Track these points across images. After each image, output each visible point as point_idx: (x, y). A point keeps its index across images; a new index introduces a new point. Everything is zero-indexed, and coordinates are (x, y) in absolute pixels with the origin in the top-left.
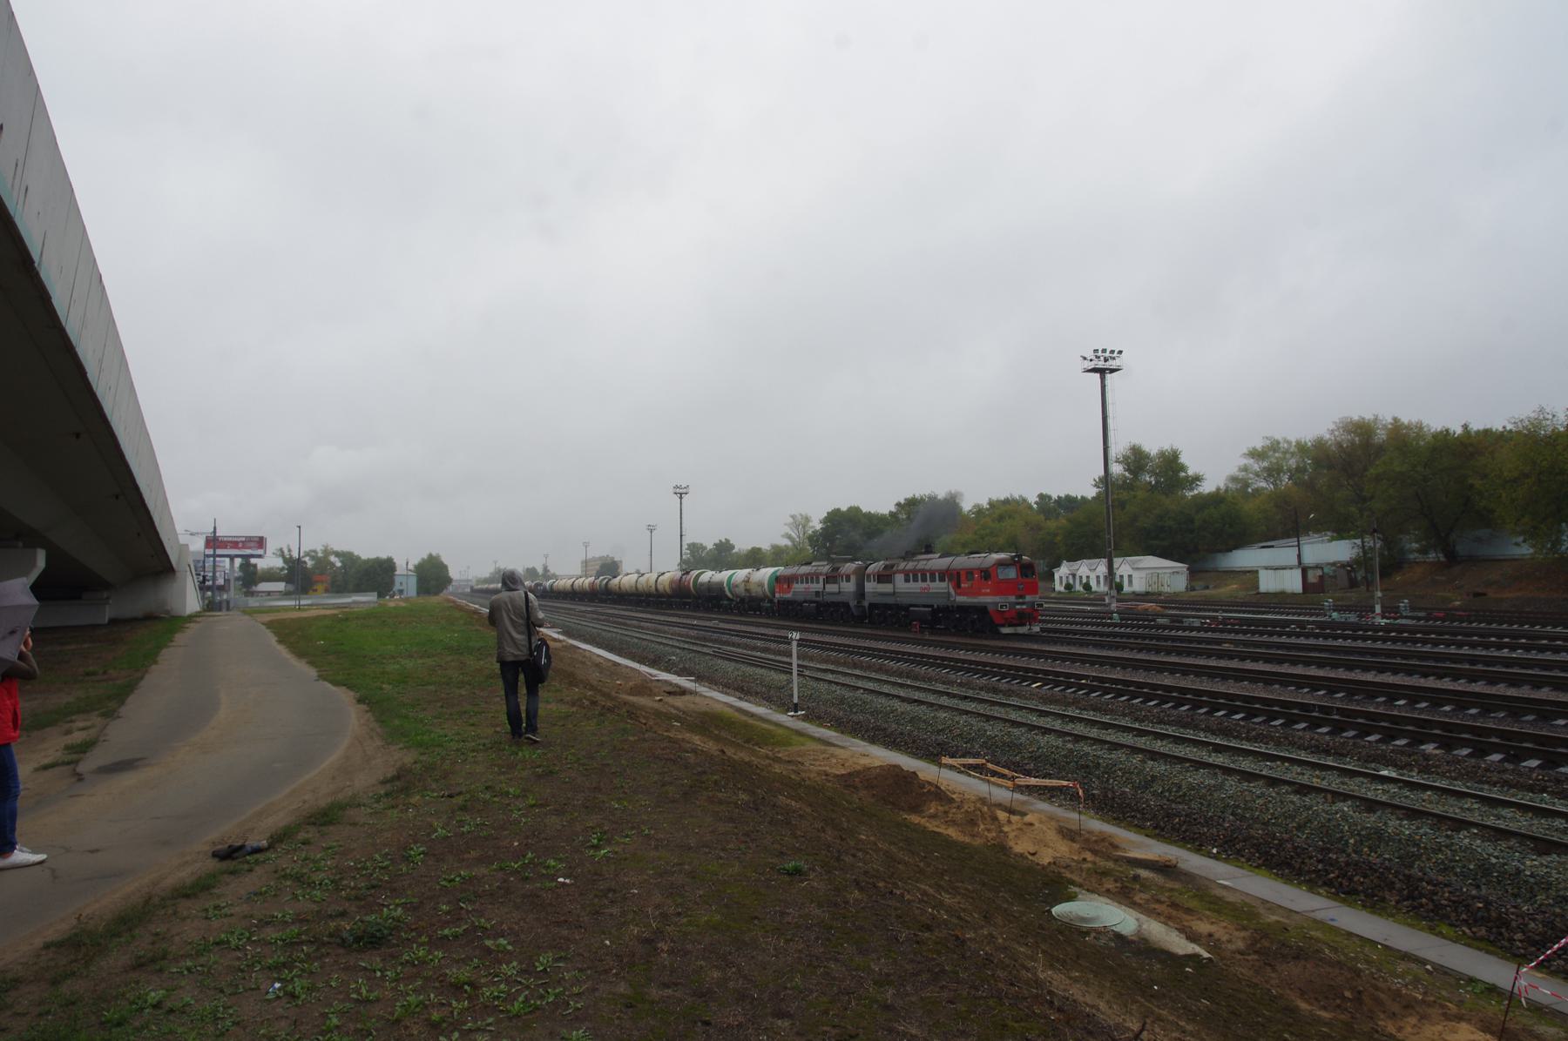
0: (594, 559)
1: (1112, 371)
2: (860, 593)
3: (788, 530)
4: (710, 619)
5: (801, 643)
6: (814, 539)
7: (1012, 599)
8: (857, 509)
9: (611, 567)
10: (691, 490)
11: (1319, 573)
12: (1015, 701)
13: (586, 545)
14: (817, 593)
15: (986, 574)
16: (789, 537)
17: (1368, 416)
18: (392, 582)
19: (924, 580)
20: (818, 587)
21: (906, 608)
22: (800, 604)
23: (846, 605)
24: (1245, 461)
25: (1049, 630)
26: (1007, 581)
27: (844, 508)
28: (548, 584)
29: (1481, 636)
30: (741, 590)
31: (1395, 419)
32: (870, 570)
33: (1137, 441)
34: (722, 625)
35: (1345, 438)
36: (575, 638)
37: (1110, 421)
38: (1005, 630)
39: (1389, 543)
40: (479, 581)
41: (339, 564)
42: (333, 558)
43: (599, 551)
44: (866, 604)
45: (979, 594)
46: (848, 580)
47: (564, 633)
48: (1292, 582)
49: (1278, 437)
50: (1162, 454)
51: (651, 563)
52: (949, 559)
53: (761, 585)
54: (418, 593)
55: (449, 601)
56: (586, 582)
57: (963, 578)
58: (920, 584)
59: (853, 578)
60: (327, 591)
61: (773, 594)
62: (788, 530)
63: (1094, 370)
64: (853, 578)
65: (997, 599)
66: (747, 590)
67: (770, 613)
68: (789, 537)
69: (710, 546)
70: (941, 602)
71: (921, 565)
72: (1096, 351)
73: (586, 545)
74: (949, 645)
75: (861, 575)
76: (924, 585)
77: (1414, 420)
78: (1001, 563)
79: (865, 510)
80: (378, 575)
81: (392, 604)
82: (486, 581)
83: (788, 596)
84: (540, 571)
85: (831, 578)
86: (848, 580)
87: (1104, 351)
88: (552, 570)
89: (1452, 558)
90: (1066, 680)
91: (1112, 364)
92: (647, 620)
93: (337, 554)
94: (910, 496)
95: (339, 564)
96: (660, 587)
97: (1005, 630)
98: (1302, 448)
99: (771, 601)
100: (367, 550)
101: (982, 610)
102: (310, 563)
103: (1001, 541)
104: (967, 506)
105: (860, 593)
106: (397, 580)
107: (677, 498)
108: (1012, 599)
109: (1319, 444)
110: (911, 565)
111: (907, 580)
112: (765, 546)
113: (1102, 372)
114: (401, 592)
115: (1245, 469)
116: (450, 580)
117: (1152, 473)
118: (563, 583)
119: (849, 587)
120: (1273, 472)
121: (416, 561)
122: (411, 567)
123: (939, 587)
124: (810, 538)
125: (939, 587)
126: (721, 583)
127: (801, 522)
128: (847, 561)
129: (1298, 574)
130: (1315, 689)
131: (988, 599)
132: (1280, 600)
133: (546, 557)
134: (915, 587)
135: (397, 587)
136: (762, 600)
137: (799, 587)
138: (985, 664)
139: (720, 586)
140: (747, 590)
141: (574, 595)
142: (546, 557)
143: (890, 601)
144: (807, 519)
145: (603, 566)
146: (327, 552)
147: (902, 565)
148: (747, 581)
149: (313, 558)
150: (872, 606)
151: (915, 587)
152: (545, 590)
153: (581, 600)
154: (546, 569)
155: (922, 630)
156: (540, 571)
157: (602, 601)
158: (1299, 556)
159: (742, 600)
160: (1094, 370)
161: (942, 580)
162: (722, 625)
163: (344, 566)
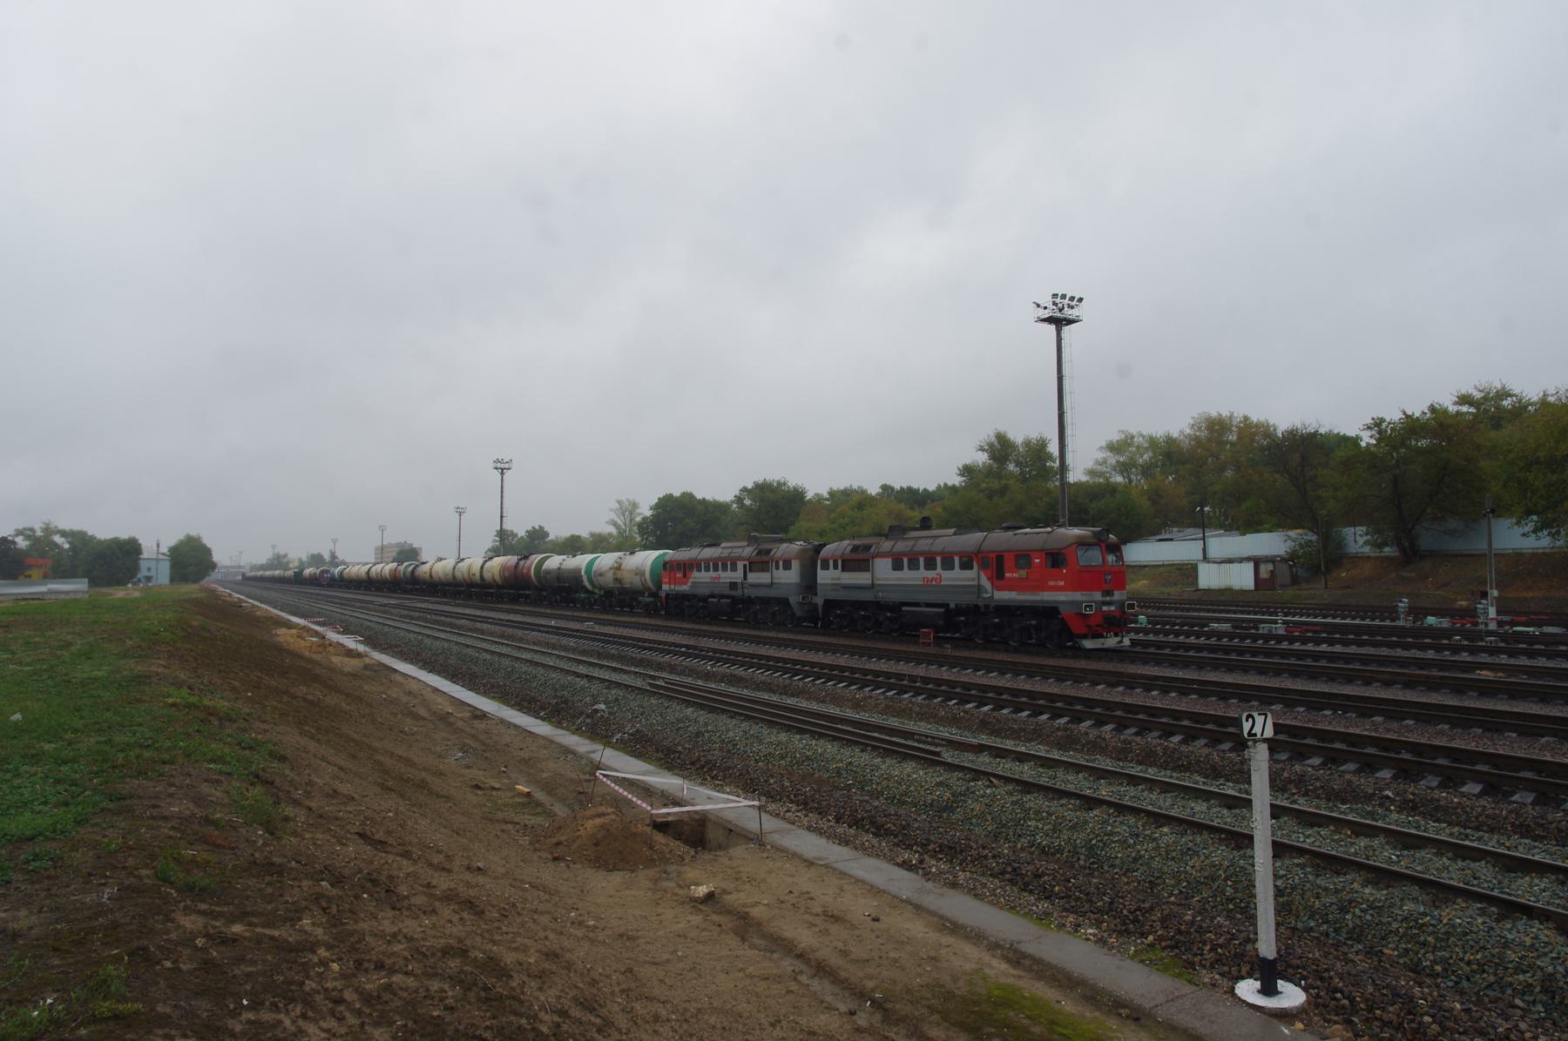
0: (391, 546)
1: (1070, 322)
2: (809, 584)
3: (613, 516)
4: (581, 620)
5: (1287, 744)
6: (643, 527)
7: (1098, 596)
8: (691, 496)
9: (408, 553)
10: (514, 465)
11: (1270, 567)
12: (1345, 811)
13: (382, 529)
14: (733, 585)
15: (1056, 558)
16: (615, 524)
17: (1225, 413)
18: (136, 568)
19: (716, 569)
20: (727, 576)
21: (896, 607)
22: (704, 599)
23: (784, 602)
24: (1100, 456)
25: (1146, 644)
26: (1088, 570)
27: (677, 494)
28: (337, 571)
29: (1314, 632)
30: (608, 580)
31: (1246, 418)
32: (824, 552)
33: (1002, 429)
34: (597, 629)
35: (1203, 434)
36: (383, 650)
37: (1066, 382)
38: (1088, 644)
39: (1326, 538)
40: (253, 568)
41: (67, 546)
42: (58, 539)
43: (394, 538)
44: (819, 601)
45: (1043, 587)
46: (787, 565)
47: (372, 641)
48: (1242, 578)
49: (1133, 431)
50: (1027, 443)
51: (459, 547)
52: (979, 535)
53: (639, 572)
54: (172, 580)
55: (213, 592)
56: (387, 568)
57: (1008, 563)
58: (712, 574)
59: (795, 564)
60: (45, 576)
61: (660, 588)
62: (613, 516)
63: (1050, 320)
64: (795, 564)
65: (1077, 596)
66: (617, 580)
67: (651, 610)
68: (615, 524)
69: (521, 533)
70: (967, 599)
71: (923, 545)
72: (1055, 296)
73: (382, 529)
74: (1016, 669)
75: (812, 561)
76: (931, 574)
77: (1262, 419)
78: (1082, 543)
79: (699, 496)
80: (115, 561)
81: (136, 594)
82: (262, 567)
83: (685, 588)
84: (327, 557)
85: (760, 562)
86: (787, 565)
87: (1063, 297)
88: (341, 556)
89: (1411, 554)
90: (1147, 719)
91: (1068, 313)
92: (485, 620)
93: (63, 534)
94: (760, 479)
95: (67, 546)
96: (487, 576)
97: (1088, 644)
98: (1153, 442)
99: (654, 595)
100: (105, 527)
101: (1049, 612)
102: (22, 543)
103: (866, 530)
104: (809, 495)
105: (809, 584)
106: (143, 565)
107: (497, 474)
108: (1098, 596)
109: (1170, 441)
110: (901, 546)
111: (897, 566)
112: (584, 533)
113: (1059, 322)
114: (149, 579)
115: (1104, 462)
116: (213, 566)
117: (1018, 464)
118: (357, 571)
119: (789, 577)
120: (1124, 468)
121: (173, 542)
122: (164, 549)
123: (957, 576)
124: (640, 526)
125: (957, 576)
126: (578, 571)
127: (629, 508)
128: (782, 541)
129: (1250, 567)
130: (1148, 689)
131: (1062, 597)
132: (1226, 599)
133: (335, 541)
134: (908, 576)
135: (143, 573)
136: (641, 593)
137: (701, 577)
138: (769, 658)
139: (575, 576)
140: (617, 580)
141: (369, 584)
142: (335, 541)
143: (867, 596)
144: (635, 505)
145: (399, 553)
146: (48, 531)
147: (887, 545)
148: (618, 568)
149: (28, 537)
150: (830, 604)
151: (908, 576)
152: (333, 579)
153: (378, 589)
154: (333, 556)
155: (939, 641)
156: (327, 557)
157: (405, 591)
158: (1204, 550)
159: (609, 593)
160: (1050, 320)
161: (966, 566)
162: (597, 629)
163: (73, 548)
